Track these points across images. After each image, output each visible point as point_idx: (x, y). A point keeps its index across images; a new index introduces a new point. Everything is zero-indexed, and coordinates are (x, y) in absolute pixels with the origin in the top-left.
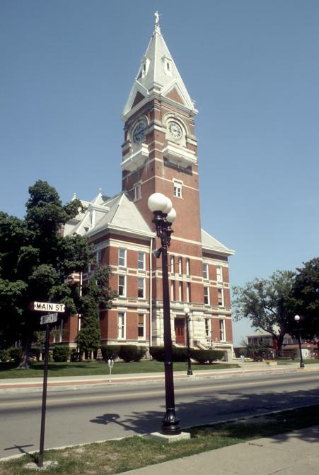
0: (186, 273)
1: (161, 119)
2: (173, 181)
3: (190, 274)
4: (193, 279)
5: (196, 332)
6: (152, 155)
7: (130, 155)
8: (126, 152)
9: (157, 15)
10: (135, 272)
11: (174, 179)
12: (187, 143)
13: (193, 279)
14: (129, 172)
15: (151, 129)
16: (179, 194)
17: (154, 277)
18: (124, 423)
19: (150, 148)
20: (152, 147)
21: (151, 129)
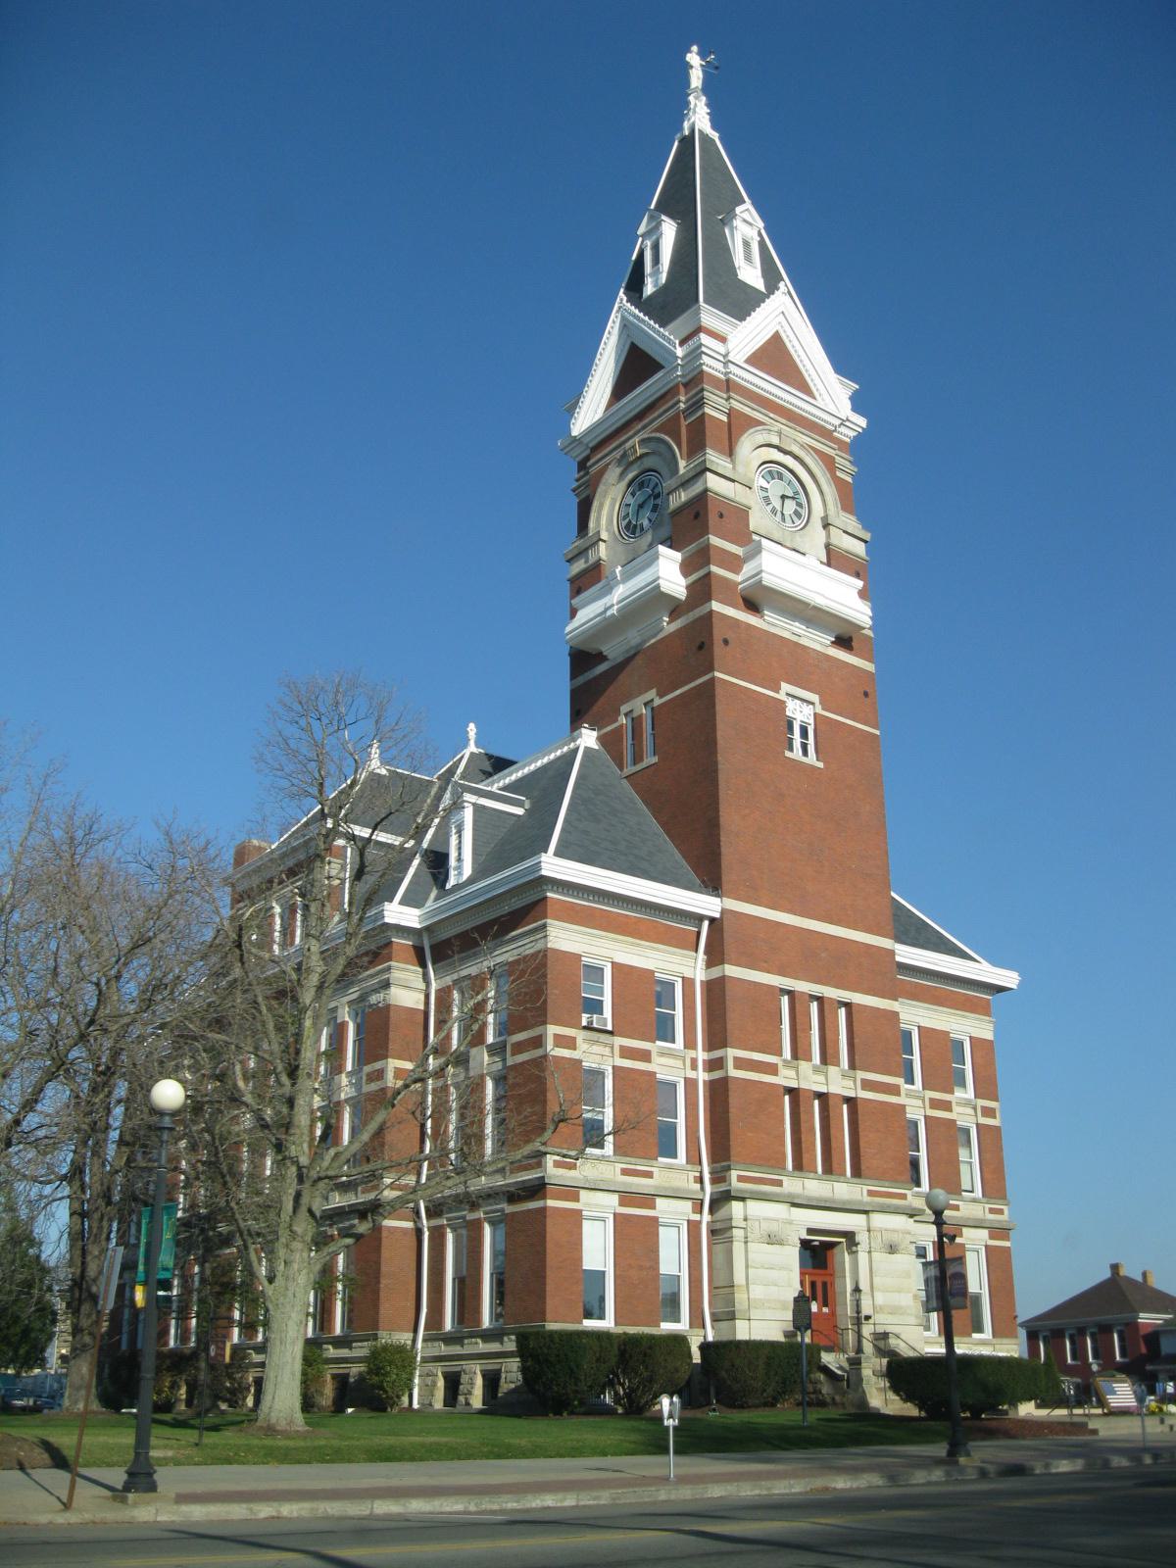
0: (809, 1059)
1: (730, 452)
2: (781, 696)
3: (853, 1066)
4: (867, 1085)
5: (880, 1298)
6: (702, 590)
7: (608, 590)
8: (590, 579)
9: (694, 58)
10: (645, 1056)
11: (785, 687)
12: (828, 546)
13: (867, 1085)
14: (600, 657)
15: (696, 489)
16: (804, 747)
17: (717, 1074)
18: (84, 1283)
19: (686, 568)
20: (696, 562)
21: (696, 489)
